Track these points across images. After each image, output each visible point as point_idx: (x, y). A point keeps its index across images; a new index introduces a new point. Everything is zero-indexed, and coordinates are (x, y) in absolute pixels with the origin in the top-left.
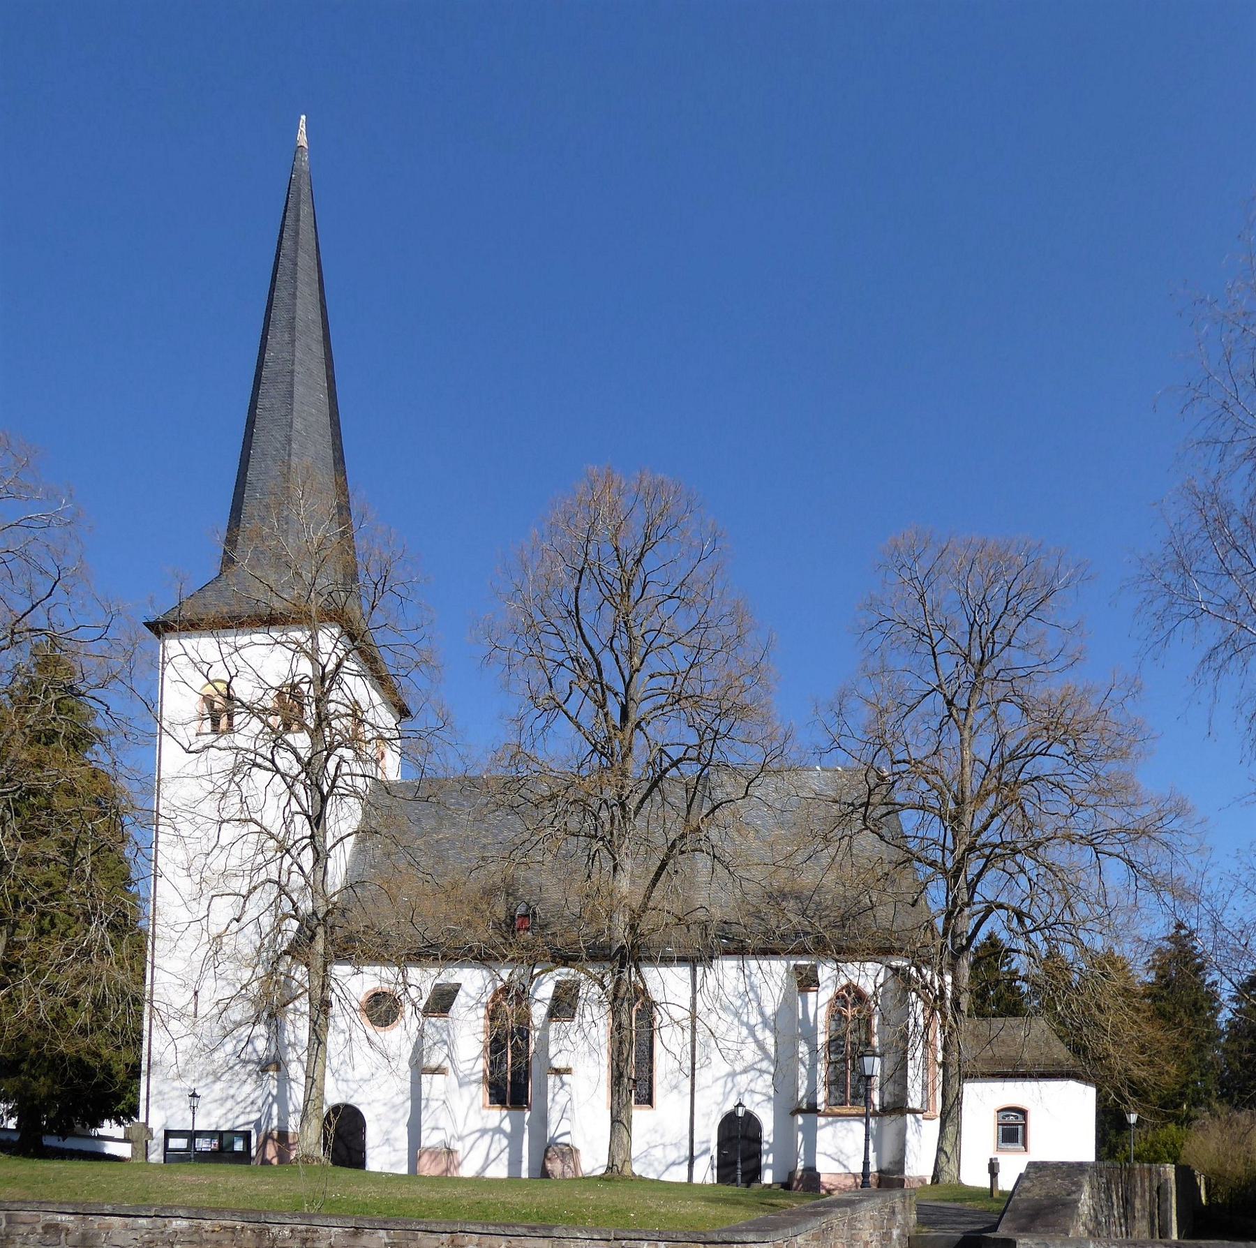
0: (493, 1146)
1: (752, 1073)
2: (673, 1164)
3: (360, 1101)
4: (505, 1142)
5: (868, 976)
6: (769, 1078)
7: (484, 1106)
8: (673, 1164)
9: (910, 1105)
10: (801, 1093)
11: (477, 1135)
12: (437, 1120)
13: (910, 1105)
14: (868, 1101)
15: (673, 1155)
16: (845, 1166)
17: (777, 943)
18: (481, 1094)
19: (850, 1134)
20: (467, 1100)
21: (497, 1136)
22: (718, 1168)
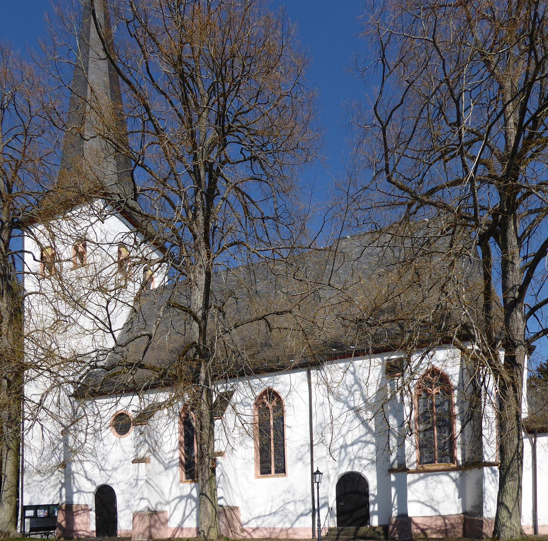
0: (187, 508)
1: (360, 444)
2: (302, 515)
3: (113, 483)
4: (194, 504)
5: (447, 361)
6: (372, 447)
7: (181, 481)
8: (302, 515)
9: (486, 459)
10: (393, 457)
11: (177, 500)
12: (143, 493)
13: (486, 459)
14: (453, 459)
15: (301, 509)
16: (436, 510)
17: (349, 337)
18: (177, 472)
19: (440, 486)
20: (171, 478)
21: (189, 501)
22: (338, 516)
